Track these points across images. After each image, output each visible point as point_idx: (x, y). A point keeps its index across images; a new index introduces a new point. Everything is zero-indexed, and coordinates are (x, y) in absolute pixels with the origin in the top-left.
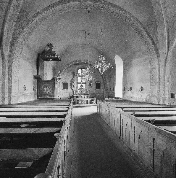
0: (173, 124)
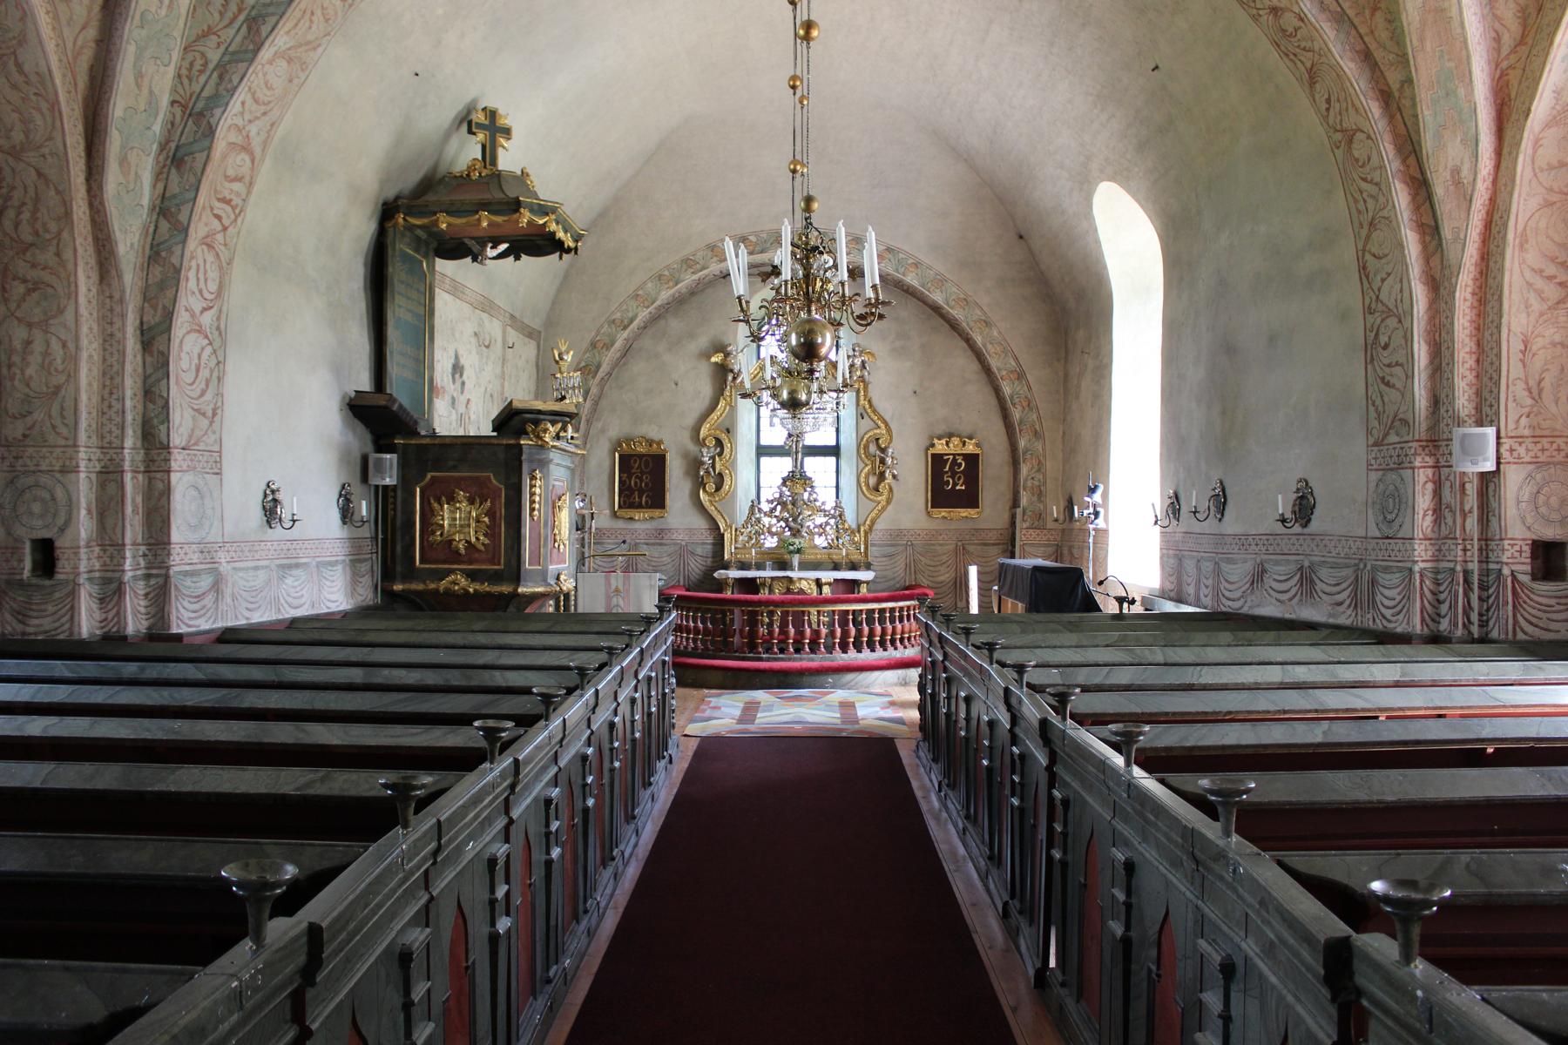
0: (1228, 752)
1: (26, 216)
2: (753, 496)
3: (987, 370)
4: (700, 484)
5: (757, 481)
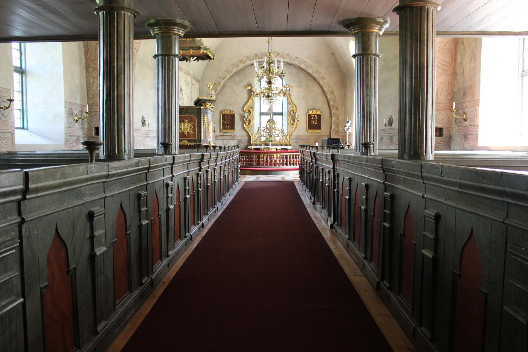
1: (93, 53)
2: (259, 126)
3: (323, 91)
4: (244, 123)
5: (259, 122)
